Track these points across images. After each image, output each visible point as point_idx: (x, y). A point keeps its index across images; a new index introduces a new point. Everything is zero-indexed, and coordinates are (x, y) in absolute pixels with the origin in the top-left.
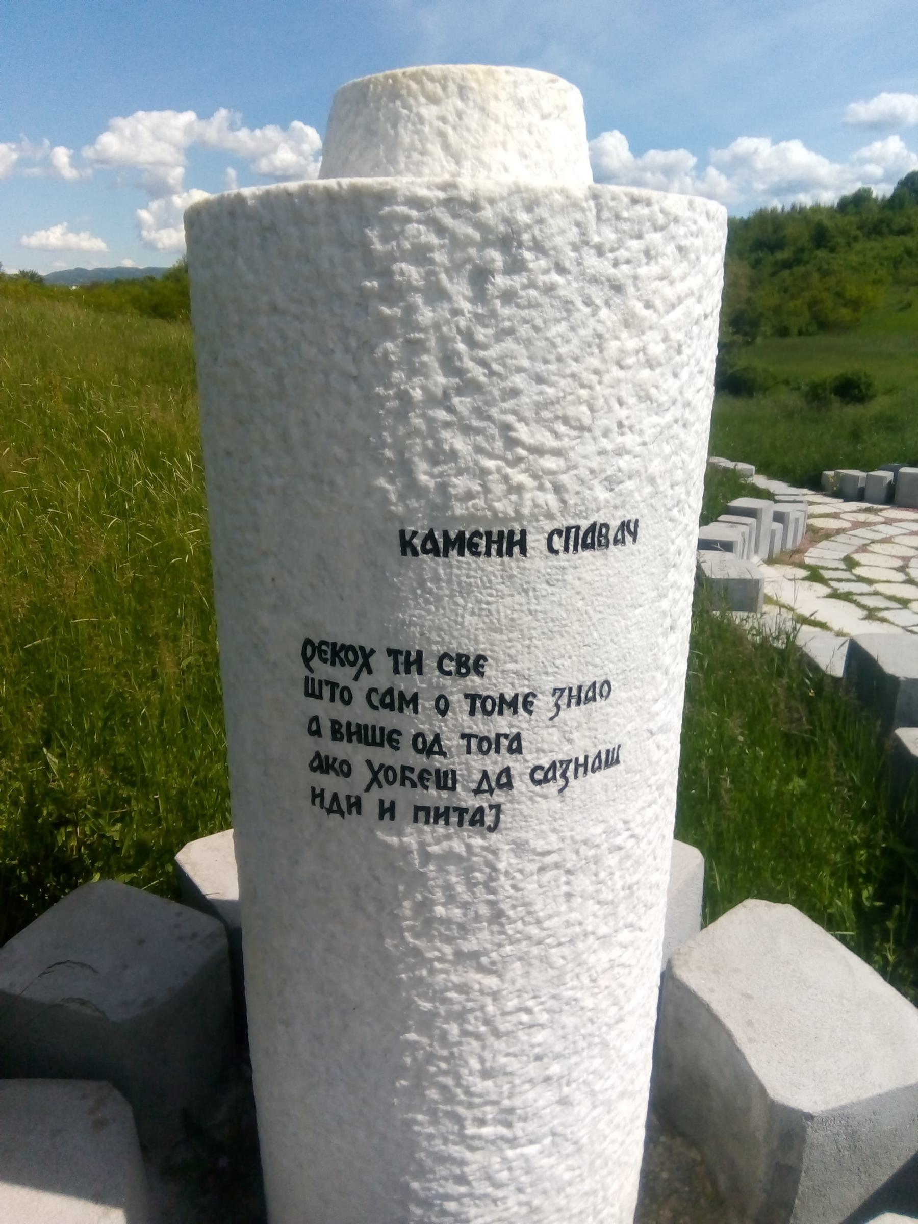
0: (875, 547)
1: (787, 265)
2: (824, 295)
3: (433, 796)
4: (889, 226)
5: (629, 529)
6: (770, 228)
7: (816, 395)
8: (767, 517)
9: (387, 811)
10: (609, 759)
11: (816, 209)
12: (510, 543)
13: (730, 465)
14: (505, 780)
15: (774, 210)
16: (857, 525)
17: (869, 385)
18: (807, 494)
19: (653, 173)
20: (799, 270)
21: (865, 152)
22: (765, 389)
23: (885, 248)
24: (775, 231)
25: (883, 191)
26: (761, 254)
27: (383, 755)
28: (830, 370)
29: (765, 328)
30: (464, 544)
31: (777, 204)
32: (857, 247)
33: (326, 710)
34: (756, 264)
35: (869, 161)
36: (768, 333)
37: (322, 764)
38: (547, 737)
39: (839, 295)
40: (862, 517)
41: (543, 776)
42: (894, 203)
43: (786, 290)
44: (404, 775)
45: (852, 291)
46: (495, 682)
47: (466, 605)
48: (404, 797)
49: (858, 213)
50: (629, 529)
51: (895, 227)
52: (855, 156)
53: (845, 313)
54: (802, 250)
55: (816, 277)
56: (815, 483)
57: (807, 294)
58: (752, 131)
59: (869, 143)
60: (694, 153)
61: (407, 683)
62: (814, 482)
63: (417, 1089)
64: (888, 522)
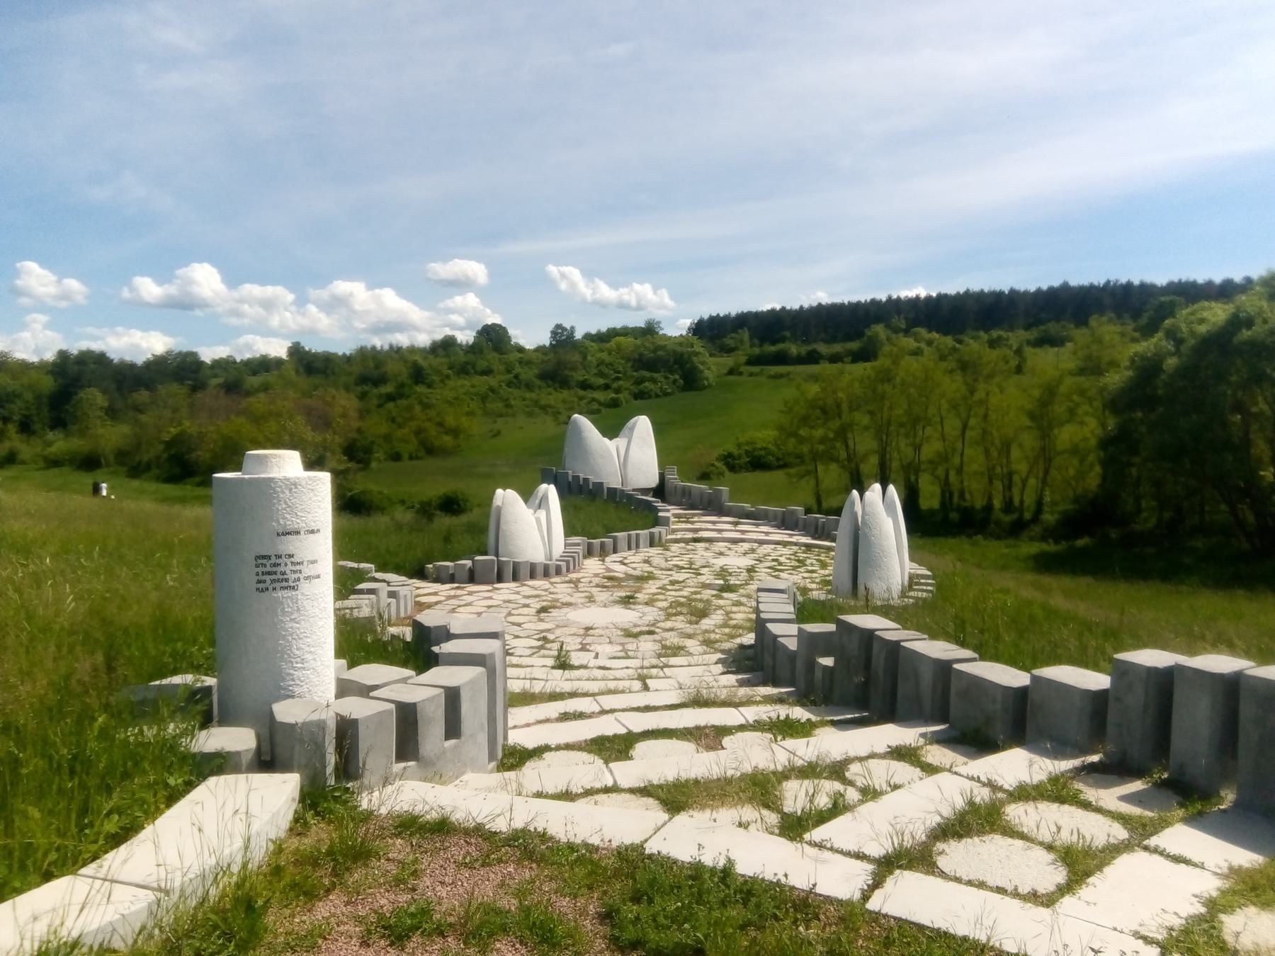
0: (461, 609)
1: (391, 398)
2: (427, 424)
3: (284, 584)
4: (474, 367)
5: (318, 531)
6: (372, 365)
7: (426, 511)
8: (383, 595)
9: (274, 589)
10: (318, 577)
11: (412, 350)
12: (298, 533)
13: (355, 565)
14: (299, 579)
15: (374, 348)
16: (449, 598)
17: (466, 501)
18: (416, 582)
19: (251, 306)
20: (403, 402)
21: (450, 303)
22: (382, 510)
23: (473, 386)
24: (377, 367)
25: (465, 337)
26: (366, 388)
27: (274, 577)
28: (435, 489)
29: (379, 454)
30: (289, 533)
31: (379, 342)
32: (451, 383)
33: (260, 570)
34: (363, 396)
35: (453, 311)
36: (382, 458)
37: (259, 582)
38: (307, 570)
39: (440, 424)
40: (452, 593)
41: (307, 578)
42: (473, 349)
43: (393, 420)
44: (278, 580)
45: (450, 421)
46: (295, 559)
47: (290, 545)
48: (277, 585)
49: (448, 356)
50: (318, 531)
51: (478, 369)
52: (441, 305)
53: (448, 440)
54: (402, 386)
55: (418, 408)
56: (420, 574)
57: (413, 424)
58: (349, 276)
59: (451, 297)
60: (292, 291)
61: (278, 561)
62: (419, 573)
63: (282, 657)
64: (470, 593)
